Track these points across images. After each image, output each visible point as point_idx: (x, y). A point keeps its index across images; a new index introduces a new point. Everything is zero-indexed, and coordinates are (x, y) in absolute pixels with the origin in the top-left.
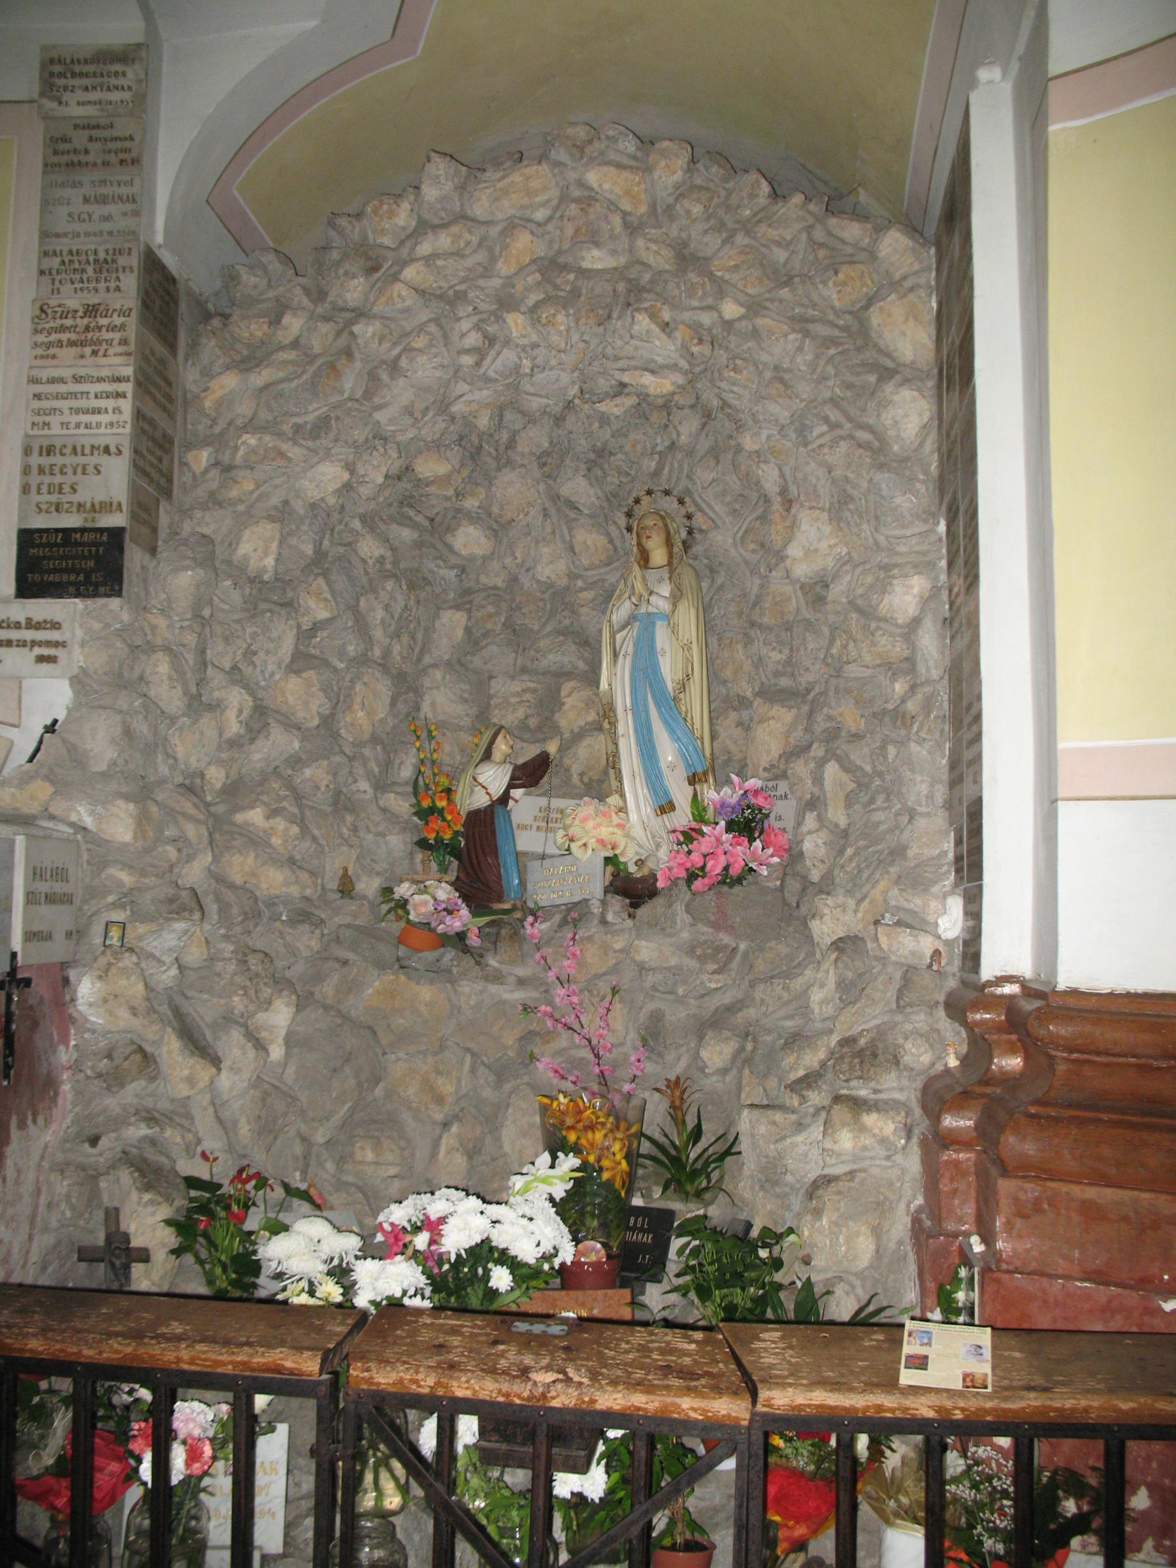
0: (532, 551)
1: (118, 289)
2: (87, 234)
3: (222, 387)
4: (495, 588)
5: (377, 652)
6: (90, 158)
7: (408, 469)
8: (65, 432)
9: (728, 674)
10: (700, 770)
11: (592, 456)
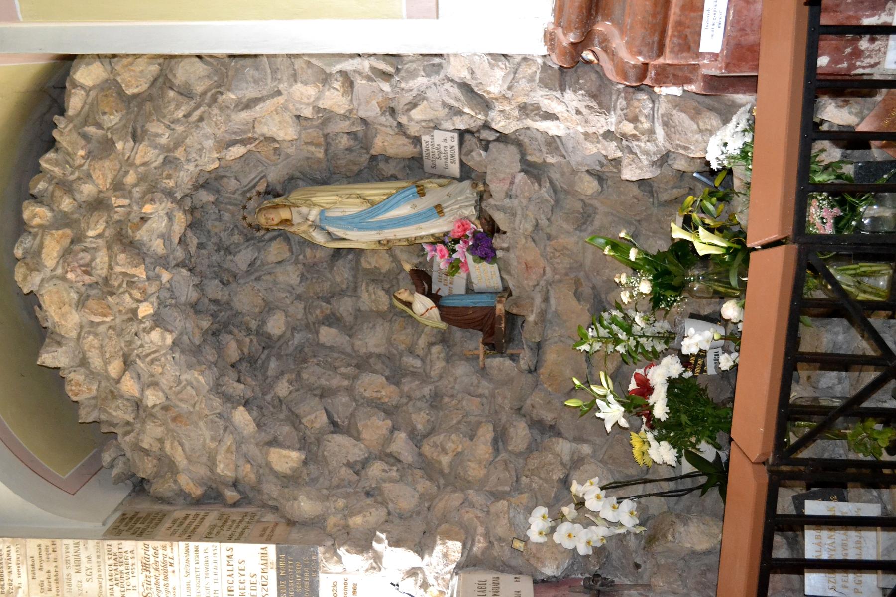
0: (282, 286)
1: (132, 552)
2: (99, 570)
3: (188, 484)
4: (305, 309)
5: (346, 383)
6: (53, 569)
7: (233, 366)
8: (219, 581)
9: (356, 168)
10: (415, 189)
11: (222, 252)
